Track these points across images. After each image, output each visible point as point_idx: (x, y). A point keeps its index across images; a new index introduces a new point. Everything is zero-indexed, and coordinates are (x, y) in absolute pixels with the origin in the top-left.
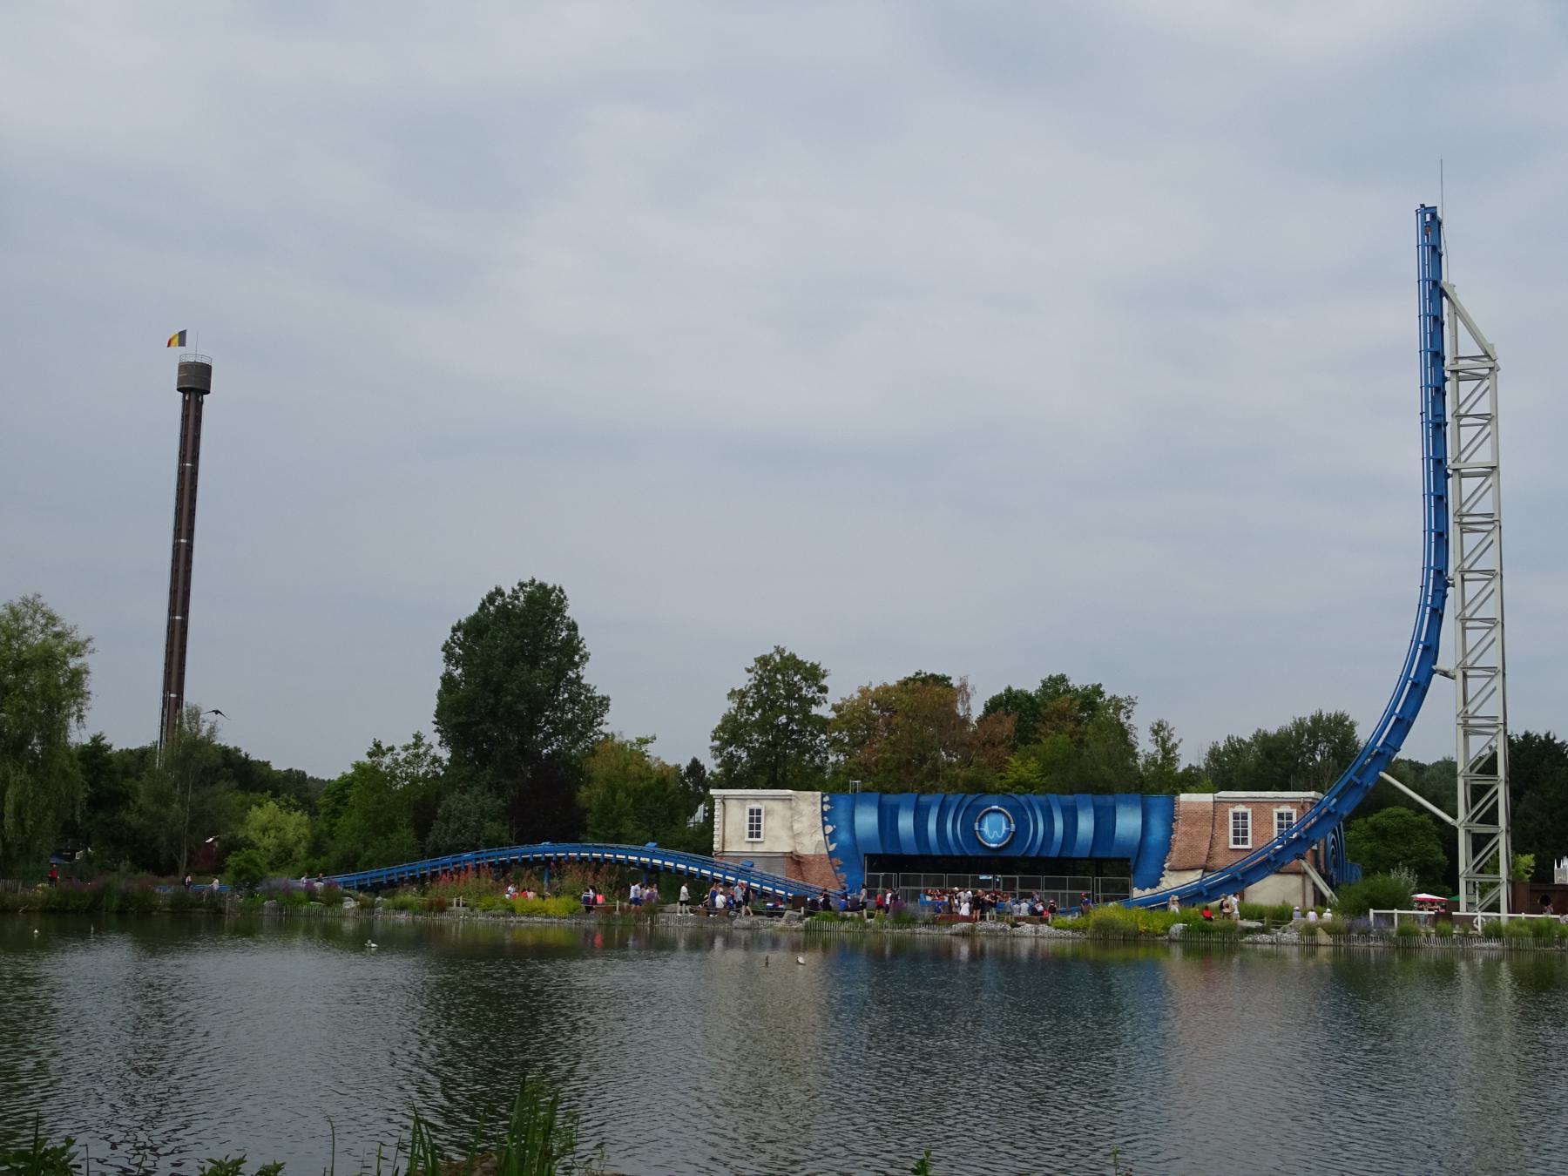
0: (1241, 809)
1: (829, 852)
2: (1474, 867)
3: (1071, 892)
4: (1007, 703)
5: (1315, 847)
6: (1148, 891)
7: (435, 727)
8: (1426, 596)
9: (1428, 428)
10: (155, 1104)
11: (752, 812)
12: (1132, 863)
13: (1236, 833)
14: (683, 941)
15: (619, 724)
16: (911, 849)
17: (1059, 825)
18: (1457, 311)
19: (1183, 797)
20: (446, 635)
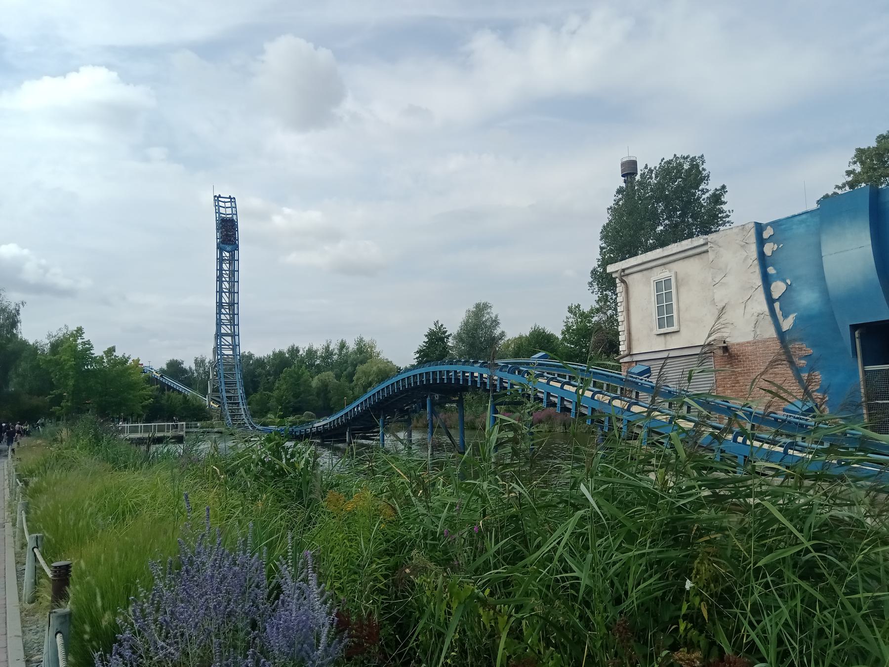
1: (781, 334)
3: (772, 586)
10: (46, 632)
11: (658, 284)
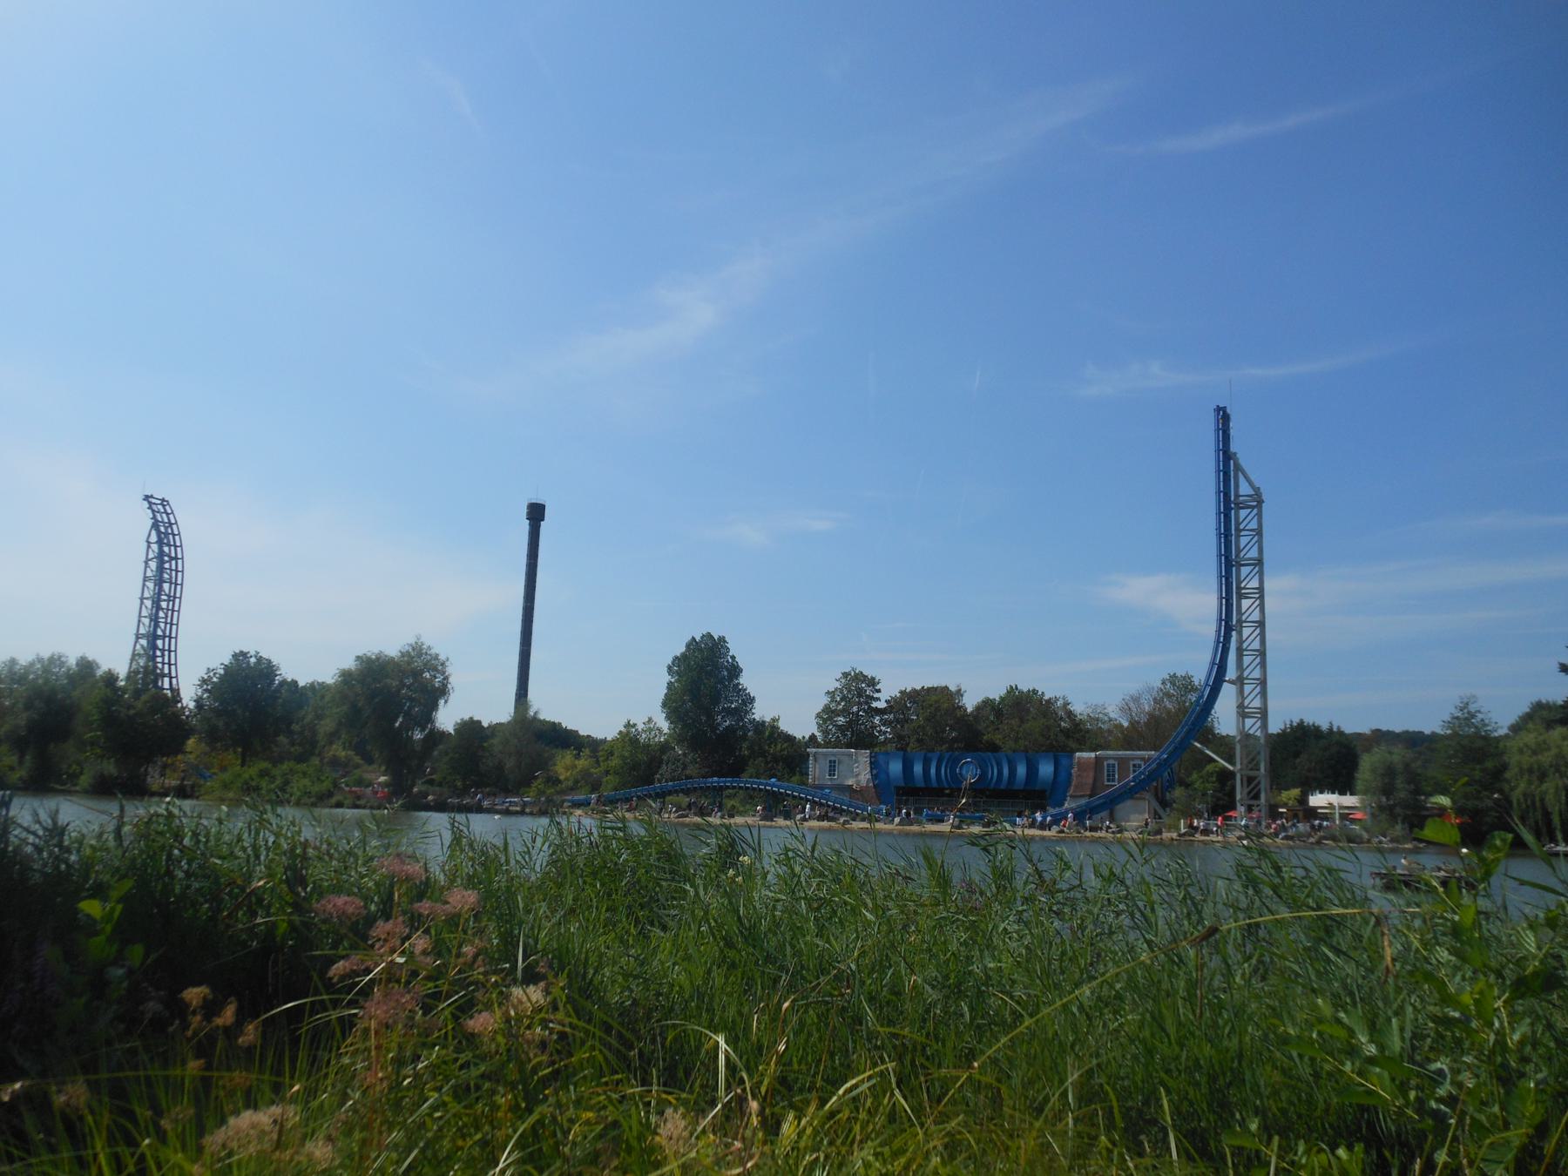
0: (1111, 762)
2: (1250, 792)
4: (672, 705)
5: (1155, 784)
6: (1057, 809)
7: (1288, 723)
8: (1219, 636)
9: (1220, 538)
11: (830, 761)
12: (1048, 793)
13: (1108, 775)
14: (1231, 953)
15: (761, 711)
16: (920, 783)
17: (1006, 771)
18: (1238, 468)
19: (1078, 754)
20: (669, 661)
